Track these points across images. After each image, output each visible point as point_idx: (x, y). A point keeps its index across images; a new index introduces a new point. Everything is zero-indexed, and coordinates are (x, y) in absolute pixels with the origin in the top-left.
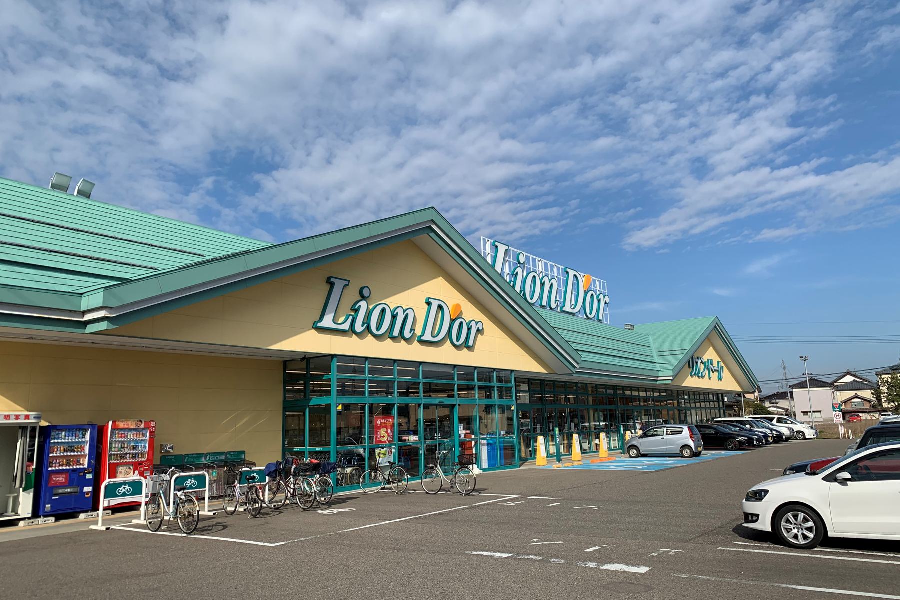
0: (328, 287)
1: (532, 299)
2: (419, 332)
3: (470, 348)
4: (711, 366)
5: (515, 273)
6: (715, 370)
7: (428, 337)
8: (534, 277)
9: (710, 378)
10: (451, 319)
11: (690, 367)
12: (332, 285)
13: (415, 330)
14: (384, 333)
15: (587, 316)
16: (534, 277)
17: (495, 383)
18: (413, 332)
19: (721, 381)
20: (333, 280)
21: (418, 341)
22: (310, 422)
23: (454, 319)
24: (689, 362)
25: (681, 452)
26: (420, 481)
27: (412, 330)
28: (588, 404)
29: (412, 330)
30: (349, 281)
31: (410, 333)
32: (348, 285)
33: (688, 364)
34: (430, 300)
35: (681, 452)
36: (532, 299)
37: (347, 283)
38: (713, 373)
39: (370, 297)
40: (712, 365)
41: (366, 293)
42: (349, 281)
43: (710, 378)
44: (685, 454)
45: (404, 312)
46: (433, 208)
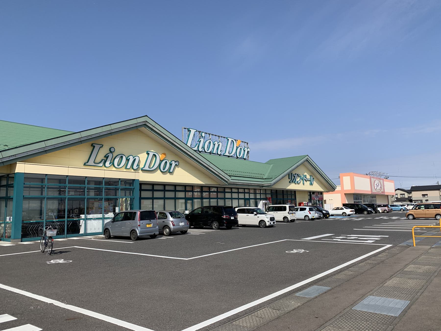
0: (92, 148)
1: (239, 156)
2: (141, 166)
3: (171, 173)
4: (304, 178)
5: (199, 141)
6: (307, 180)
7: (147, 168)
8: (241, 148)
9: (303, 184)
10: (160, 160)
11: (289, 178)
12: (94, 147)
13: (139, 166)
14: (167, 171)
15: (237, 156)
16: (241, 148)
17: (103, 186)
18: (138, 166)
19: (312, 186)
20: (94, 145)
21: (141, 170)
22: (280, 204)
23: (162, 160)
24: (289, 174)
25: (401, 210)
26: (53, 249)
27: (138, 165)
28: (25, 198)
29: (138, 165)
30: (103, 145)
31: (137, 167)
32: (102, 147)
33: (288, 175)
34: (148, 152)
35: (401, 210)
36: (239, 156)
37: (102, 146)
38: (306, 181)
39: (114, 152)
40: (306, 178)
41: (112, 150)
42: (103, 145)
43: (303, 184)
44: (402, 210)
45: (133, 158)
46: (146, 116)
